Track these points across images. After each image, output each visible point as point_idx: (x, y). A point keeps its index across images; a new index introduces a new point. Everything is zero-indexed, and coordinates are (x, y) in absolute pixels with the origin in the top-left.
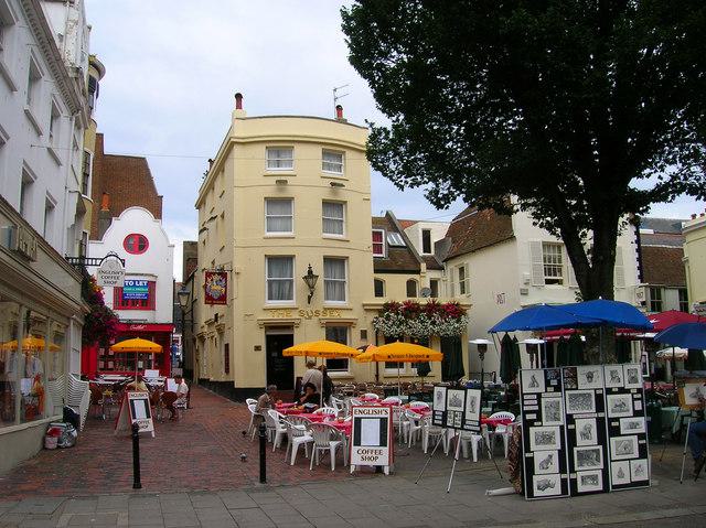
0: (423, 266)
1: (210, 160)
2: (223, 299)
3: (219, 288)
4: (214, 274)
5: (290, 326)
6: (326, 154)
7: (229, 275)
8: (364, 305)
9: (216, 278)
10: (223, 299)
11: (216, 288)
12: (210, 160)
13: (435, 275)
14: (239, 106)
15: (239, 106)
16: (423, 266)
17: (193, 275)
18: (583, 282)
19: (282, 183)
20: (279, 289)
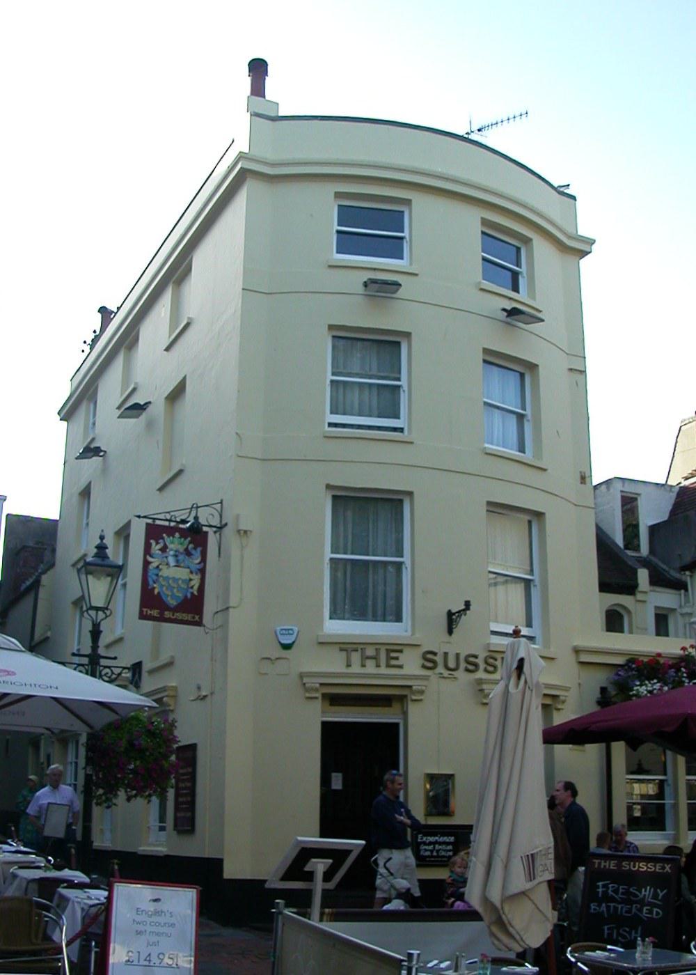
0: (643, 575)
1: (103, 310)
2: (191, 608)
3: (182, 573)
4: (171, 531)
5: (395, 698)
6: (491, 234)
7: (212, 540)
8: (577, 651)
9: (175, 544)
10: (191, 608)
11: (174, 574)
12: (103, 310)
13: (665, 598)
14: (258, 89)
15: (258, 89)
16: (643, 575)
17: (36, 584)
18: (111, 705)
19: (382, 289)
20: (366, 588)
